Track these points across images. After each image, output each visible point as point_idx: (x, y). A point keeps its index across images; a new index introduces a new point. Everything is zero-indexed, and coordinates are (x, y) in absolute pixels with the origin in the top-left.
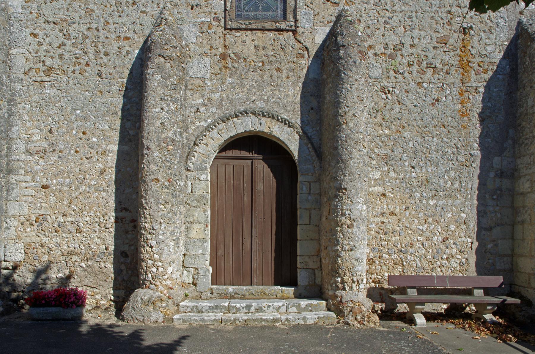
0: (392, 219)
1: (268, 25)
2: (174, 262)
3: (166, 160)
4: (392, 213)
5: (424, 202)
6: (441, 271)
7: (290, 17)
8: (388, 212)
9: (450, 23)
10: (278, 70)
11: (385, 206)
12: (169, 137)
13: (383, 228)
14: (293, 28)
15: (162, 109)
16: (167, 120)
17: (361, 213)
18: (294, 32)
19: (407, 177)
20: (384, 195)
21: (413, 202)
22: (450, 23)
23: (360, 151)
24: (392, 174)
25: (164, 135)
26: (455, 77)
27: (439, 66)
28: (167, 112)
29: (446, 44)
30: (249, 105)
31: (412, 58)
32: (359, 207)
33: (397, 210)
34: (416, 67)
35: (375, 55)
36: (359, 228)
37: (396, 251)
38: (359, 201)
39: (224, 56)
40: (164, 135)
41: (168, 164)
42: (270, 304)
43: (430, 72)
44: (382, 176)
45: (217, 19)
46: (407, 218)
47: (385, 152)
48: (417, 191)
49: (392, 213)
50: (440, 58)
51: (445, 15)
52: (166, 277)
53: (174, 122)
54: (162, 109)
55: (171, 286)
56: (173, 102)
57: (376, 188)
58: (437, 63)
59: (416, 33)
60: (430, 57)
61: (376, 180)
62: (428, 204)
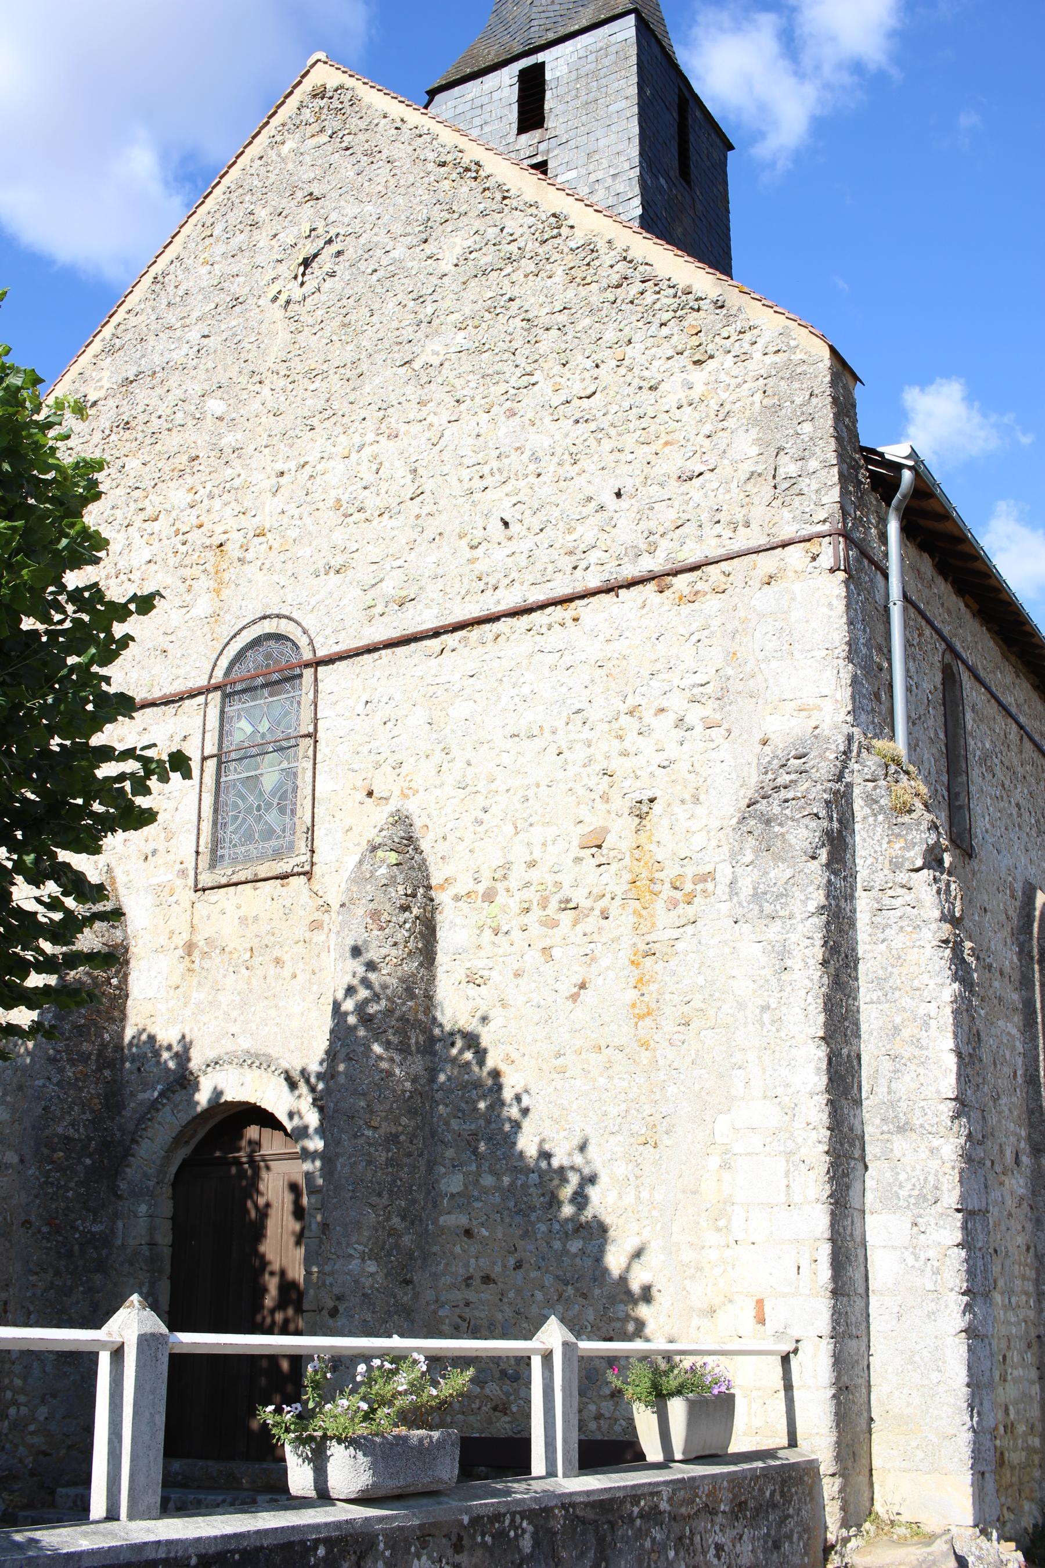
0: (488, 1294)
1: (263, 871)
2: (54, 1396)
3: (46, 1183)
4: (487, 1279)
5: (557, 1245)
6: (599, 1428)
7: (302, 846)
8: (478, 1276)
9: (605, 798)
10: (278, 961)
11: (473, 1261)
12: (57, 1135)
13: (467, 1316)
14: (307, 868)
15: (49, 1079)
16: (55, 1101)
17: (356, 1282)
18: (309, 874)
19: (519, 1183)
20: (468, 1233)
21: (531, 1247)
22: (605, 798)
23: (355, 1136)
24: (488, 1180)
25: (47, 1132)
26: (622, 921)
27: (585, 904)
28: (57, 1084)
29: (599, 847)
30: (227, 1045)
31: (530, 894)
32: (355, 1264)
33: (498, 1269)
34: (536, 912)
35: (457, 898)
36: (352, 1316)
37: (497, 1375)
38: (352, 1252)
39: (190, 947)
40: (47, 1132)
41: (50, 1190)
42: (202, 1497)
43: (567, 917)
44: (466, 1187)
45: (183, 873)
46: (519, 1291)
47: (473, 1127)
48: (539, 1219)
49: (487, 1279)
50: (585, 880)
51: (596, 779)
52: (32, 1428)
53: (73, 1102)
54: (49, 1079)
55: (44, 1448)
56: (72, 1062)
57: (453, 1217)
58: (579, 897)
59: (537, 834)
60: (566, 885)
61: (453, 1195)
62: (565, 1251)
